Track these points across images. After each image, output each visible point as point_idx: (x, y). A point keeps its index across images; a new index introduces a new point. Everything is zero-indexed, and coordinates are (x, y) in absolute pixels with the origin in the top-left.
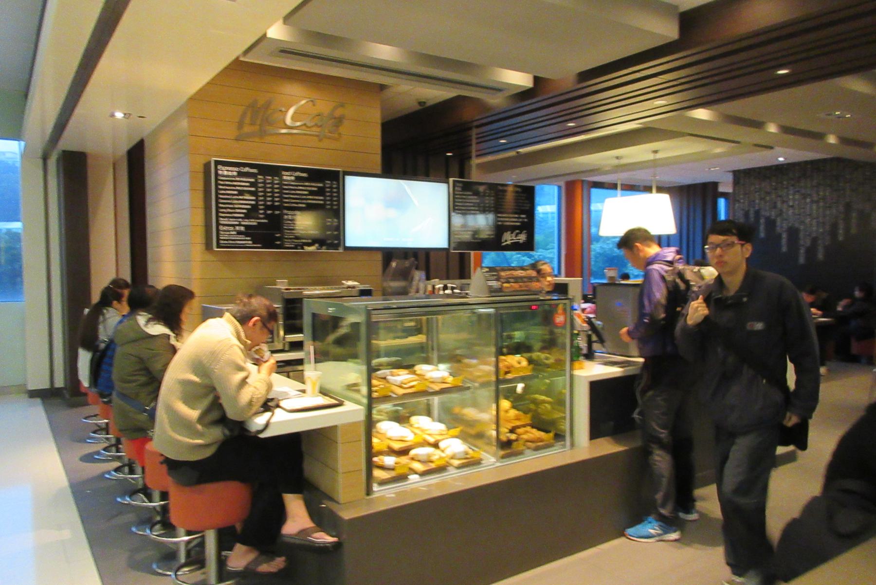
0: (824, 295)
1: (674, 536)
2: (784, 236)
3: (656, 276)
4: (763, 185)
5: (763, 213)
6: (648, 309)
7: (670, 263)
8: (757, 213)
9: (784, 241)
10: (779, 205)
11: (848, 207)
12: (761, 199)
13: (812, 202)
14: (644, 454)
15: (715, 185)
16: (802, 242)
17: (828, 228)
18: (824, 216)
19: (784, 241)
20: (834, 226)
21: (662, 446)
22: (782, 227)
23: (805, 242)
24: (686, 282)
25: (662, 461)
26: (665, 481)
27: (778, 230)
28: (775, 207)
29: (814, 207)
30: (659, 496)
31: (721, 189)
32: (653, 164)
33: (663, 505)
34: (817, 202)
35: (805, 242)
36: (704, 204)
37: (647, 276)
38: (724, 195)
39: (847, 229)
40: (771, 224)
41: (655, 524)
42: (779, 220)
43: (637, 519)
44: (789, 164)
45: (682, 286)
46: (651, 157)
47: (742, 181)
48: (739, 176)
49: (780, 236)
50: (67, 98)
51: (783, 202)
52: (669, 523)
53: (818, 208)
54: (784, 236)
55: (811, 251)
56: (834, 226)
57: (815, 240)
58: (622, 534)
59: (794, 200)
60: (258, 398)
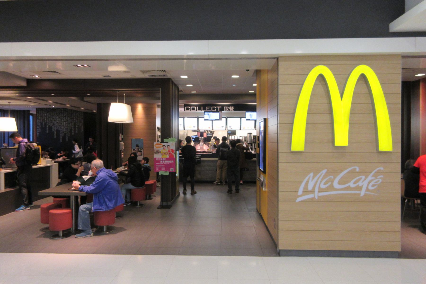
0: (68, 152)
1: (29, 208)
2: (55, 132)
3: (23, 146)
4: (48, 114)
5: (47, 124)
6: (21, 154)
7: (26, 143)
8: (45, 124)
9: (55, 134)
10: (53, 121)
11: (75, 124)
12: (47, 119)
13: (64, 121)
14: (20, 189)
15: (28, 111)
16: (61, 135)
17: (69, 130)
18: (68, 126)
19: (55, 134)
20: (71, 130)
21: (25, 187)
22: (54, 129)
23: (62, 135)
24: (31, 148)
25: (25, 191)
26: (26, 196)
27: (53, 130)
28: (52, 122)
29: (65, 123)
30: (24, 199)
31: (31, 112)
32: (9, 105)
33: (25, 201)
34: (66, 122)
35: (62, 135)
36: (24, 118)
37: (20, 146)
38: (32, 115)
39: (75, 131)
40: (50, 128)
41: (24, 206)
42: (53, 127)
43: (18, 206)
44: (56, 108)
45: (30, 148)
46: (8, 103)
47: (40, 112)
48: (38, 110)
49: (54, 132)
51: (54, 121)
52: (27, 206)
53: (66, 123)
54: (55, 132)
55: (64, 138)
56: (71, 130)
57: (65, 134)
58: (14, 211)
59: (58, 120)
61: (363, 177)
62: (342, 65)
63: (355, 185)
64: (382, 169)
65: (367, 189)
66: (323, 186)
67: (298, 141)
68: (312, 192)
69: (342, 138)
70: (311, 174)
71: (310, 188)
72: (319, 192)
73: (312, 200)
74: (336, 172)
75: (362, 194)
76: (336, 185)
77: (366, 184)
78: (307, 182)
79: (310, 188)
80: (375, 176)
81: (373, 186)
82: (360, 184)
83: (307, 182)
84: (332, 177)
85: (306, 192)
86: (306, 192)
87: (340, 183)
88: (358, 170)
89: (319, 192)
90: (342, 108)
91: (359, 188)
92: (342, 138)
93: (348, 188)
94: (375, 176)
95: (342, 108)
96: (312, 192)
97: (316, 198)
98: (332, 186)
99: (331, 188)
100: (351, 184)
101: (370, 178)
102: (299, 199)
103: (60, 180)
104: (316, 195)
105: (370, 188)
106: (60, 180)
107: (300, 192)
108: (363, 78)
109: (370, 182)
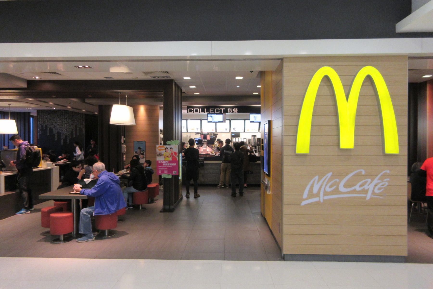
0: (69, 155)
1: (29, 212)
2: (56, 134)
3: (23, 149)
4: (48, 116)
5: (48, 126)
6: (21, 157)
7: (27, 145)
8: (46, 126)
9: (56, 136)
10: (54, 123)
11: (76, 126)
12: (47, 121)
13: (65, 124)
14: (21, 193)
15: (29, 113)
16: (62, 137)
17: (70, 133)
18: (69, 128)
19: (56, 136)
20: (72, 132)
21: (25, 190)
22: (55, 131)
23: (63, 137)
24: (31, 150)
25: (25, 194)
26: (26, 199)
27: (54, 133)
28: (53, 124)
29: (66, 125)
30: (25, 203)
31: (32, 114)
32: (9, 107)
33: (26, 205)
34: (67, 124)
35: (63, 137)
36: (25, 120)
37: (20, 149)
38: (33, 117)
39: (76, 133)
40: (51, 130)
41: (24, 210)
42: (54, 129)
43: (18, 210)
44: (57, 110)
45: (30, 151)
46: (8, 105)
47: (40, 114)
48: (39, 112)
49: (54, 134)
50: (349, 261)
51: (55, 123)
52: (27, 209)
53: (67, 126)
54: (56, 134)
55: (65, 140)
56: (72, 132)
57: (66, 137)
58: (15, 215)
59: (59, 122)
60: (249, 140)
61: (369, 180)
62: (348, 66)
63: (361, 188)
64: (388, 172)
65: (373, 193)
66: (328, 190)
67: (303, 144)
68: (318, 195)
69: (347, 140)
70: (317, 178)
71: (315, 191)
72: (324, 195)
73: (318, 204)
74: (341, 175)
75: (368, 197)
76: (342, 188)
77: (372, 187)
78: (312, 185)
79: (315, 191)
80: (381, 179)
81: (379, 189)
82: (366, 187)
83: (312, 185)
84: (338, 180)
85: (311, 195)
86: (311, 195)
87: (345, 186)
88: (363, 173)
89: (324, 195)
90: (348, 110)
91: (365, 192)
92: (347, 140)
93: (354, 191)
94: (381, 179)
95: (348, 110)
96: (318, 195)
97: (322, 201)
98: (337, 189)
99: (336, 191)
100: (357, 188)
101: (376, 181)
102: (304, 203)
103: (61, 183)
104: (322, 198)
105: (376, 191)
106: (61, 183)
107: (305, 195)
108: (369, 79)
109: (376, 185)
